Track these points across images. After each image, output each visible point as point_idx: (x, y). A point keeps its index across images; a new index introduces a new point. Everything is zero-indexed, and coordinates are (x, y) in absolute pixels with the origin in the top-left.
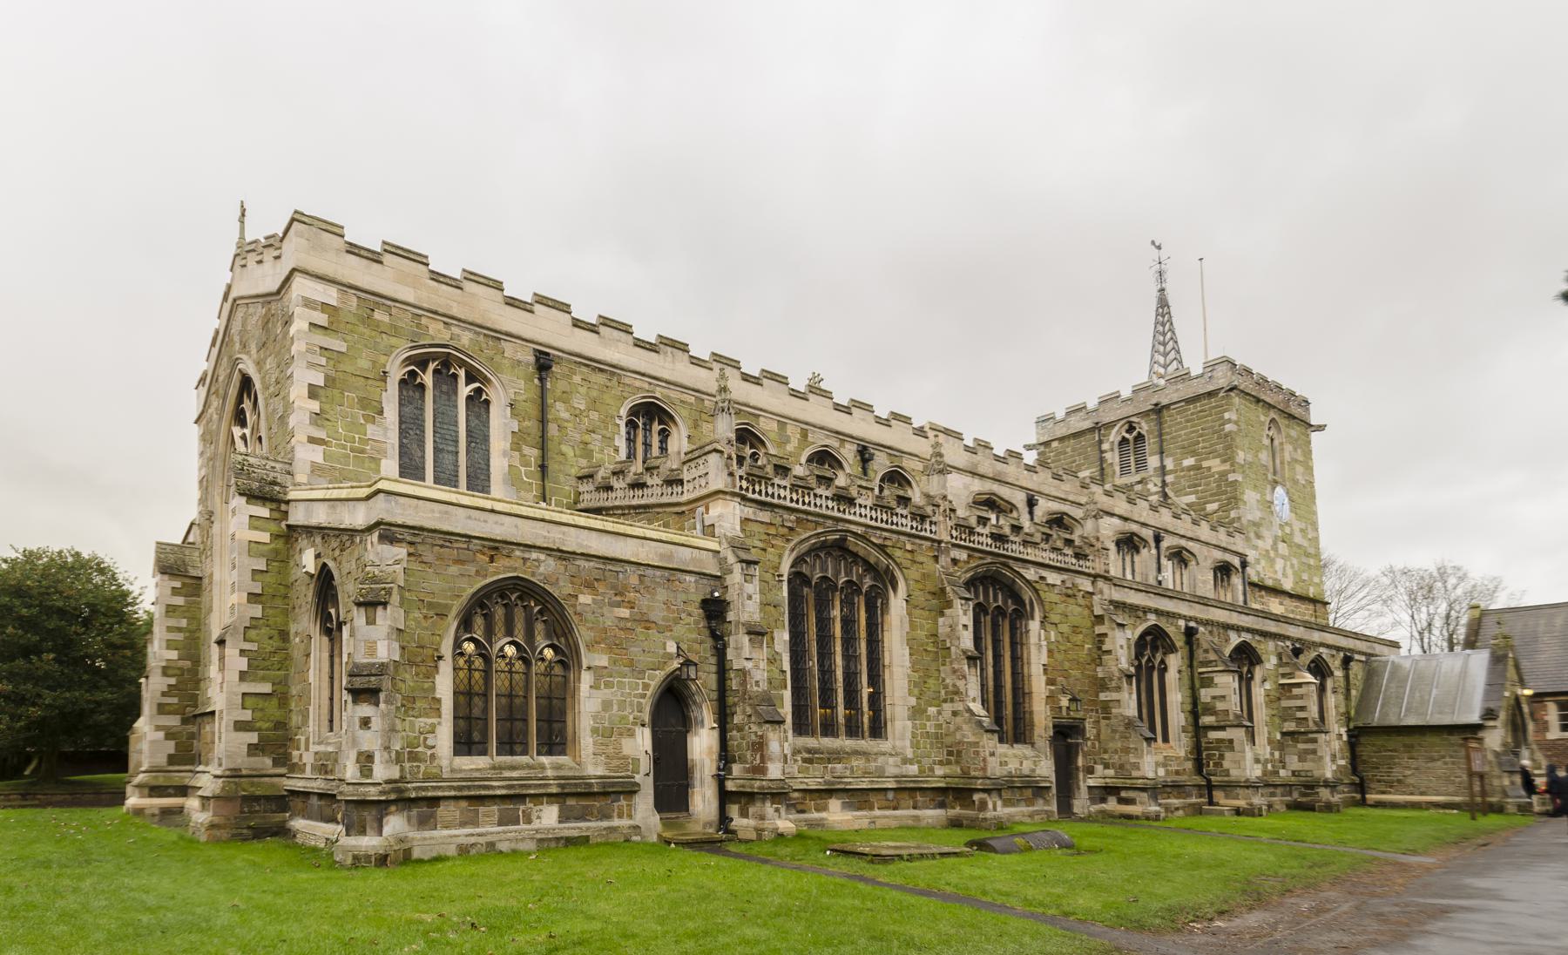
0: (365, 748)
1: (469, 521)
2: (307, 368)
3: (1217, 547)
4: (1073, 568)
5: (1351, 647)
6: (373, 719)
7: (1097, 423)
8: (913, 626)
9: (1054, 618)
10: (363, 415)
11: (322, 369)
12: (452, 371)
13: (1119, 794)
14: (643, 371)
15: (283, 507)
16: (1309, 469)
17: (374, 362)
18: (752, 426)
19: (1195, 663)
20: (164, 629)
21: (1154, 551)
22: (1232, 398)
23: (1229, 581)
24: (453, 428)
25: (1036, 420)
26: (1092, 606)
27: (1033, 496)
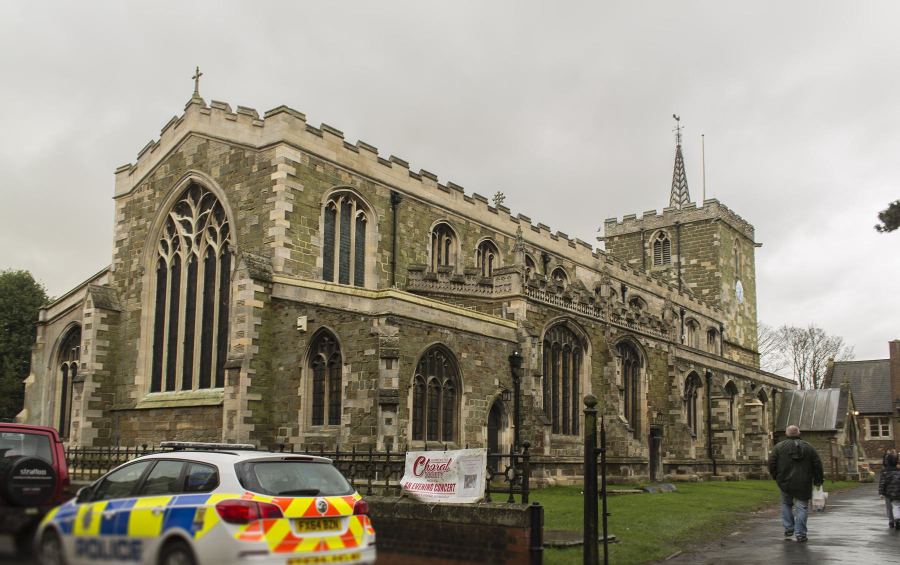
0: (389, 434)
1: (422, 313)
2: (285, 201)
3: (709, 318)
4: (660, 338)
5: (776, 384)
6: (393, 419)
7: (642, 229)
8: (593, 372)
9: (652, 367)
10: (310, 230)
11: (291, 201)
12: (350, 202)
13: (677, 468)
14: (442, 204)
15: (270, 286)
16: (753, 270)
17: (315, 197)
18: (493, 240)
19: (710, 393)
20: (95, 347)
21: (680, 321)
22: (718, 225)
23: (714, 339)
24: (347, 237)
26: (667, 360)
27: (625, 285)
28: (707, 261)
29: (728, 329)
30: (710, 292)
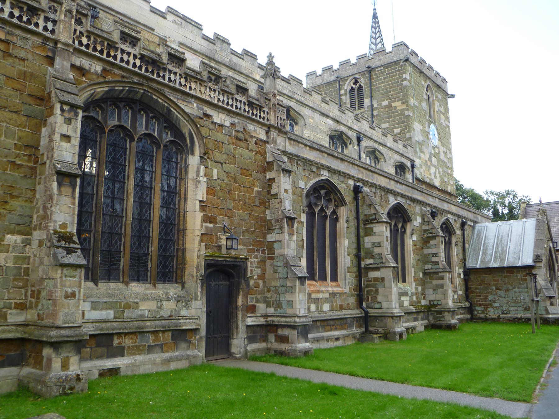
3: (397, 152)
7: (338, 77)
13: (277, 332)
16: (447, 119)
21: (356, 147)
25: (306, 75)
28: (398, 101)
29: (422, 168)
30: (401, 131)
